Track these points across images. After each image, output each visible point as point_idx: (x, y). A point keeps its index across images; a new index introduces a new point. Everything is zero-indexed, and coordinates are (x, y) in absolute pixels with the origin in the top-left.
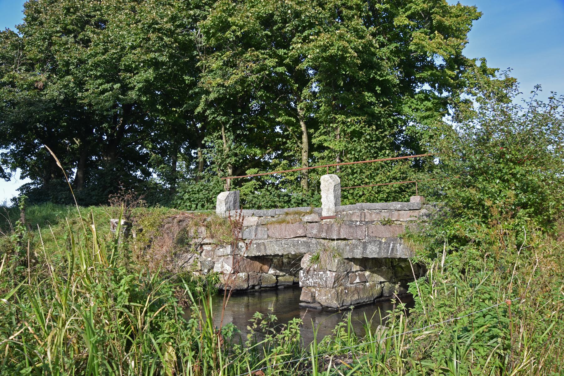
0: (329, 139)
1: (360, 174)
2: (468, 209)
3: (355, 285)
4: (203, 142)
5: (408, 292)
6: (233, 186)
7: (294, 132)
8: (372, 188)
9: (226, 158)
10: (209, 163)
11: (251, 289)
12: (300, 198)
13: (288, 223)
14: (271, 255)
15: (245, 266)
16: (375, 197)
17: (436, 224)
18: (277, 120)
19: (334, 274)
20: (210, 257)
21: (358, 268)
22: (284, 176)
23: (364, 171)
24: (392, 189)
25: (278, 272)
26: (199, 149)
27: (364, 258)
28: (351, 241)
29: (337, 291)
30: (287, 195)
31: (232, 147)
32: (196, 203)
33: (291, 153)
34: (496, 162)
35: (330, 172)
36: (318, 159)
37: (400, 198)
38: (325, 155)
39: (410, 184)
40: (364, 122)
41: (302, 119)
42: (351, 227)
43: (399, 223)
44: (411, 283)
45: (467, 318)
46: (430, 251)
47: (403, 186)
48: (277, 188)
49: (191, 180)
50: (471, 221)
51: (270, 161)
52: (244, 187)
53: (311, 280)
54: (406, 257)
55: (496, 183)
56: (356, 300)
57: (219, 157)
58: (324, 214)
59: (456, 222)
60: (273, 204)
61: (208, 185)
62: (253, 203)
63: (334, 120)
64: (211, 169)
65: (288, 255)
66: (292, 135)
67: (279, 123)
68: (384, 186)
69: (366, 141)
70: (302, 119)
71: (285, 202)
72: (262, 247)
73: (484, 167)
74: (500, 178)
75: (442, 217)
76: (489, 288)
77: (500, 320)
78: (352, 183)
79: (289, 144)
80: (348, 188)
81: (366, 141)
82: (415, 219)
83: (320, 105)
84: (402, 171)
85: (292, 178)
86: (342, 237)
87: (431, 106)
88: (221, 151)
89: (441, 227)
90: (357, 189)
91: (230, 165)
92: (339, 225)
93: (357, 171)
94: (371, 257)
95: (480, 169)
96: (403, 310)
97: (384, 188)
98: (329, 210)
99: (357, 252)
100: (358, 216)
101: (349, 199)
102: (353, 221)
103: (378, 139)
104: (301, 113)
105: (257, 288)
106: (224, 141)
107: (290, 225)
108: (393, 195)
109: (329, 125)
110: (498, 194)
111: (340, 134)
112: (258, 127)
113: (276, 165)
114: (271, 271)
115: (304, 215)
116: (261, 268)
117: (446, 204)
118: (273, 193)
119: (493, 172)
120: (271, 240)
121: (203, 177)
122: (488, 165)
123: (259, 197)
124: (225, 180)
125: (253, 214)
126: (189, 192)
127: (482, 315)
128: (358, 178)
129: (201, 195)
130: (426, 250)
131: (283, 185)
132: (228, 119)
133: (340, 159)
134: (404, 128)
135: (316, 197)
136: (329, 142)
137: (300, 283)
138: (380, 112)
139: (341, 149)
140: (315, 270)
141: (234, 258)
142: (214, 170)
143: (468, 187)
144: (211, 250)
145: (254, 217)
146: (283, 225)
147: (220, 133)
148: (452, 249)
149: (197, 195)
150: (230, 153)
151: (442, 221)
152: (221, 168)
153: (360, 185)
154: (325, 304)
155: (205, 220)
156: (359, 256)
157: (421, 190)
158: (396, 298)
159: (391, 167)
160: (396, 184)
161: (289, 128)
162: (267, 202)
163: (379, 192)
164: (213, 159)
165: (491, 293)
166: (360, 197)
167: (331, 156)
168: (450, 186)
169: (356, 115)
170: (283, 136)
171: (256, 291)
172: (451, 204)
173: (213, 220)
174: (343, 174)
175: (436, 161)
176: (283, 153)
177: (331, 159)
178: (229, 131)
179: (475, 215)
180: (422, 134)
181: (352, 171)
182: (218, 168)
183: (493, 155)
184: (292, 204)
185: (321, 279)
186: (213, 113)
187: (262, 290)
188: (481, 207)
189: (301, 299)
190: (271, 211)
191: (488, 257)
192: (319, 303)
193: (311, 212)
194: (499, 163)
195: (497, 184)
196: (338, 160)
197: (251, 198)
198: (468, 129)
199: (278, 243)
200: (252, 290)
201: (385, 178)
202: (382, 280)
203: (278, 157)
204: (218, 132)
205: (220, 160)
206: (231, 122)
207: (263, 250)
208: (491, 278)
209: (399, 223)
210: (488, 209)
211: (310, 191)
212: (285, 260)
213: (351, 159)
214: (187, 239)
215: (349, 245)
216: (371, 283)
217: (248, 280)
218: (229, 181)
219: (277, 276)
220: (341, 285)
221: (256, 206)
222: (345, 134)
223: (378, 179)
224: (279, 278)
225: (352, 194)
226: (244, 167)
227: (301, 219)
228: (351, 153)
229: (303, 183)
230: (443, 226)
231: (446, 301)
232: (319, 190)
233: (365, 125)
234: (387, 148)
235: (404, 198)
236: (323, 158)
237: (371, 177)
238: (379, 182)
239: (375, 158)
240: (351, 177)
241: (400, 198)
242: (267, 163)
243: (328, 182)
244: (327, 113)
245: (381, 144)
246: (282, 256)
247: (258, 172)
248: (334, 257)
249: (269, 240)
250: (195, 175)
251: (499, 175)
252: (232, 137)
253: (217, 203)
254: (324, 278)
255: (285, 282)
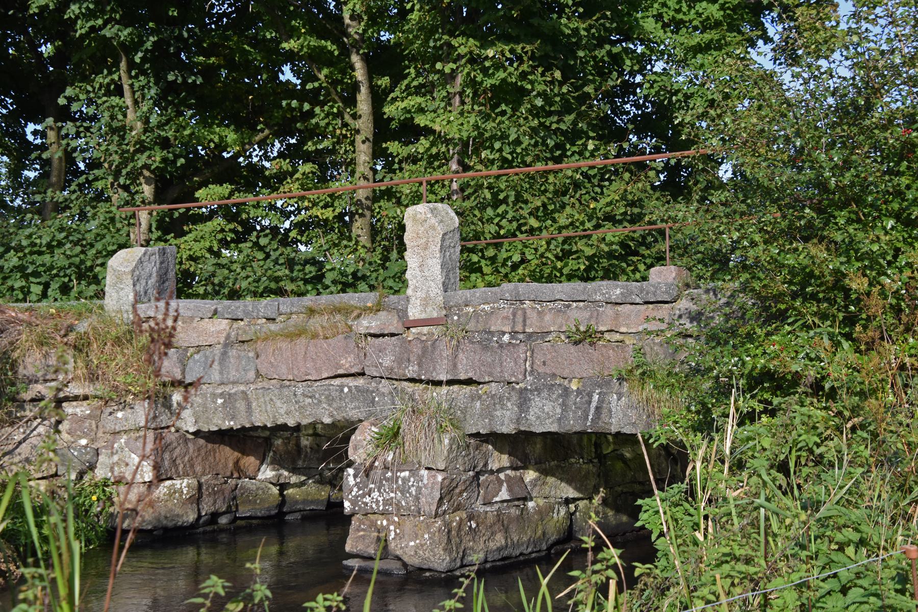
0: (432, 106)
1: (515, 204)
2: (805, 300)
3: (496, 507)
4: (62, 101)
5: (638, 524)
6: (156, 234)
7: (335, 83)
8: (548, 243)
9: (136, 151)
10: (82, 166)
11: (207, 523)
12: (350, 270)
13: (315, 336)
14: (265, 427)
15: (191, 460)
16: (555, 268)
17: (715, 339)
18: (285, 45)
19: (440, 478)
20: (85, 435)
21: (505, 460)
22: (307, 209)
23: (526, 196)
24: (603, 246)
25: (286, 473)
26: (50, 121)
27: (520, 433)
28: (486, 387)
29: (448, 525)
30: (312, 261)
31: (154, 120)
32: (42, 280)
33: (326, 144)
34: (890, 172)
35: (432, 197)
36: (400, 162)
37: (624, 271)
38: (421, 150)
39: (650, 234)
40: (532, 58)
41: (356, 45)
42: (486, 348)
43: (618, 337)
44: (647, 500)
45: (795, 595)
46: (698, 412)
47: (633, 239)
48: (285, 241)
49: (26, 211)
50: (812, 333)
51: (267, 164)
52: (188, 237)
53: (375, 494)
54: (634, 432)
55: (884, 228)
56: (499, 549)
57: (113, 148)
58: (414, 313)
59: (768, 334)
60: (273, 285)
61: (82, 228)
62: (216, 281)
63: (447, 53)
64: (87, 181)
65: (313, 425)
66: (328, 94)
67: (291, 57)
68: (581, 238)
69: (535, 112)
70: (356, 45)
71: (306, 282)
72: (241, 405)
73: (853, 184)
74: (897, 216)
75: (732, 322)
76: (856, 514)
77: (887, 602)
78: (493, 228)
79: (319, 118)
80: (482, 244)
81: (535, 112)
82: (663, 326)
83: (409, 6)
84: (630, 197)
85: (329, 214)
86: (462, 377)
87: (719, 15)
88: (120, 131)
89: (729, 347)
90: (506, 246)
91: (146, 173)
92: (454, 342)
93: (507, 197)
94: (539, 429)
95: (841, 189)
96: (615, 567)
97: (581, 245)
98: (426, 302)
99: (503, 416)
100: (506, 318)
101: (483, 275)
102: (491, 333)
103: (567, 108)
104: (355, 29)
105: (223, 520)
106: (129, 101)
107: (321, 342)
108: (605, 263)
109: (433, 66)
110: (889, 258)
111: (461, 94)
112: (231, 65)
113: (281, 177)
114: (267, 473)
115: (359, 316)
116: (237, 463)
117: (744, 288)
118: (274, 255)
119: (876, 199)
120: (265, 384)
121: (60, 207)
122: (865, 179)
123: (234, 267)
124: (134, 216)
125: (215, 312)
126: (19, 248)
127: (837, 587)
128: (509, 216)
129: (59, 259)
130: (689, 411)
131: (301, 233)
132: (140, 37)
133: (460, 163)
134: (639, 79)
135: (393, 267)
136: (430, 116)
137: (347, 504)
138: (576, 31)
139: (465, 135)
140: (386, 468)
141: (159, 438)
142: (100, 185)
143: (806, 240)
144: (90, 417)
145: (216, 321)
146: (302, 341)
147: (116, 77)
148: (759, 407)
149: (47, 258)
150: (147, 138)
151: (733, 332)
152: (122, 181)
153: (515, 236)
154: (414, 561)
155: (70, 329)
156: (507, 428)
157: (682, 250)
158: (595, 532)
159: (601, 187)
160: (613, 234)
161: (320, 71)
162: (258, 281)
163: (565, 255)
164: (96, 154)
165: (863, 528)
166: (515, 267)
167: (438, 154)
168: (757, 238)
169: (507, 38)
170: (302, 95)
171: (222, 530)
172: (757, 285)
173: (94, 329)
174: (468, 204)
175: (725, 172)
176: (302, 143)
177: (436, 164)
178: (143, 72)
179: (824, 317)
180: (687, 97)
181: (495, 195)
182: (110, 179)
183: (882, 151)
184: (327, 287)
185: (404, 491)
186: (90, 15)
187: (239, 528)
188: (841, 295)
189: (348, 548)
190: (267, 305)
191: (853, 429)
192: (398, 558)
193: (378, 308)
194: (899, 174)
195: (886, 233)
196: (454, 166)
197: (211, 269)
198: (815, 78)
199: (286, 392)
200: (208, 528)
201: (582, 217)
202: (572, 493)
203: (290, 153)
204: (110, 73)
205: (116, 158)
206: (148, 45)
207: (243, 413)
208: (863, 487)
209: (618, 337)
210: (858, 300)
211: (379, 250)
212: (305, 442)
213: (492, 162)
214: (13, 384)
215: (480, 397)
216: (541, 502)
217: (197, 498)
218: (143, 216)
219: (283, 487)
220: (457, 509)
221: (226, 291)
222: (475, 94)
223: (563, 220)
224: (289, 492)
225: (493, 259)
226: (191, 180)
227: (350, 327)
228: (492, 148)
229: (360, 228)
230: (734, 346)
231: (736, 547)
232: (402, 248)
233: (534, 68)
234: (591, 134)
235: (633, 272)
236: (414, 159)
237: (544, 214)
238: (566, 227)
239: (558, 160)
240: (490, 212)
241: (624, 271)
242: (256, 171)
243: (426, 225)
244: (429, 32)
245: (575, 123)
246: (298, 428)
247: (231, 194)
248: (441, 429)
249: (260, 385)
250: (38, 198)
251: (896, 206)
252: (153, 92)
253: (109, 280)
254: (413, 490)
255: (305, 502)
